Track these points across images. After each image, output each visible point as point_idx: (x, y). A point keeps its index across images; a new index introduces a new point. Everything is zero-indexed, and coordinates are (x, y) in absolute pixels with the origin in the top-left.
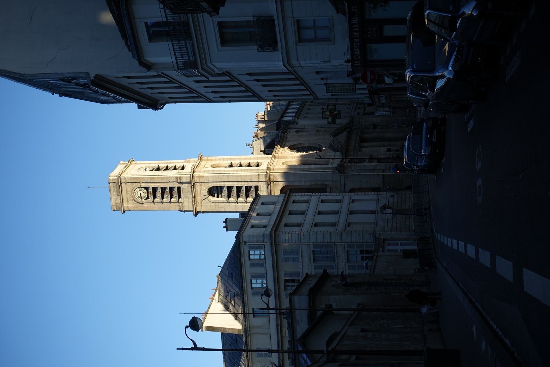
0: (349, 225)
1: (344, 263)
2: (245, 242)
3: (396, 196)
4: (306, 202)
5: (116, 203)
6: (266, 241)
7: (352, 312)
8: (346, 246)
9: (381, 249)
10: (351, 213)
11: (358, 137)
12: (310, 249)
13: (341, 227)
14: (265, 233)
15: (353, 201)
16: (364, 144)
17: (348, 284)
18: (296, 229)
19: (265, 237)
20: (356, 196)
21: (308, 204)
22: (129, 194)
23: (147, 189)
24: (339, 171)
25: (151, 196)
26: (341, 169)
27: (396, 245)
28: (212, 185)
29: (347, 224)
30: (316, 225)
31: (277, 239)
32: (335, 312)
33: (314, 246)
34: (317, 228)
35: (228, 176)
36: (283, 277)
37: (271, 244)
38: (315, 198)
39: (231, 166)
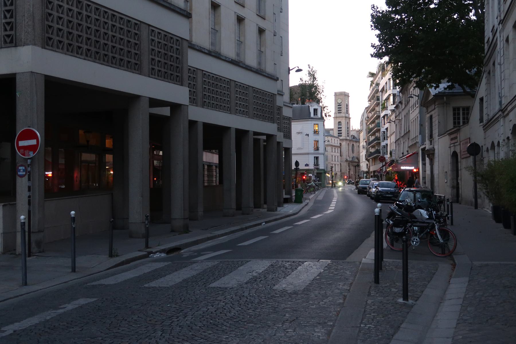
20: (339, 165)
38: (339, 154)
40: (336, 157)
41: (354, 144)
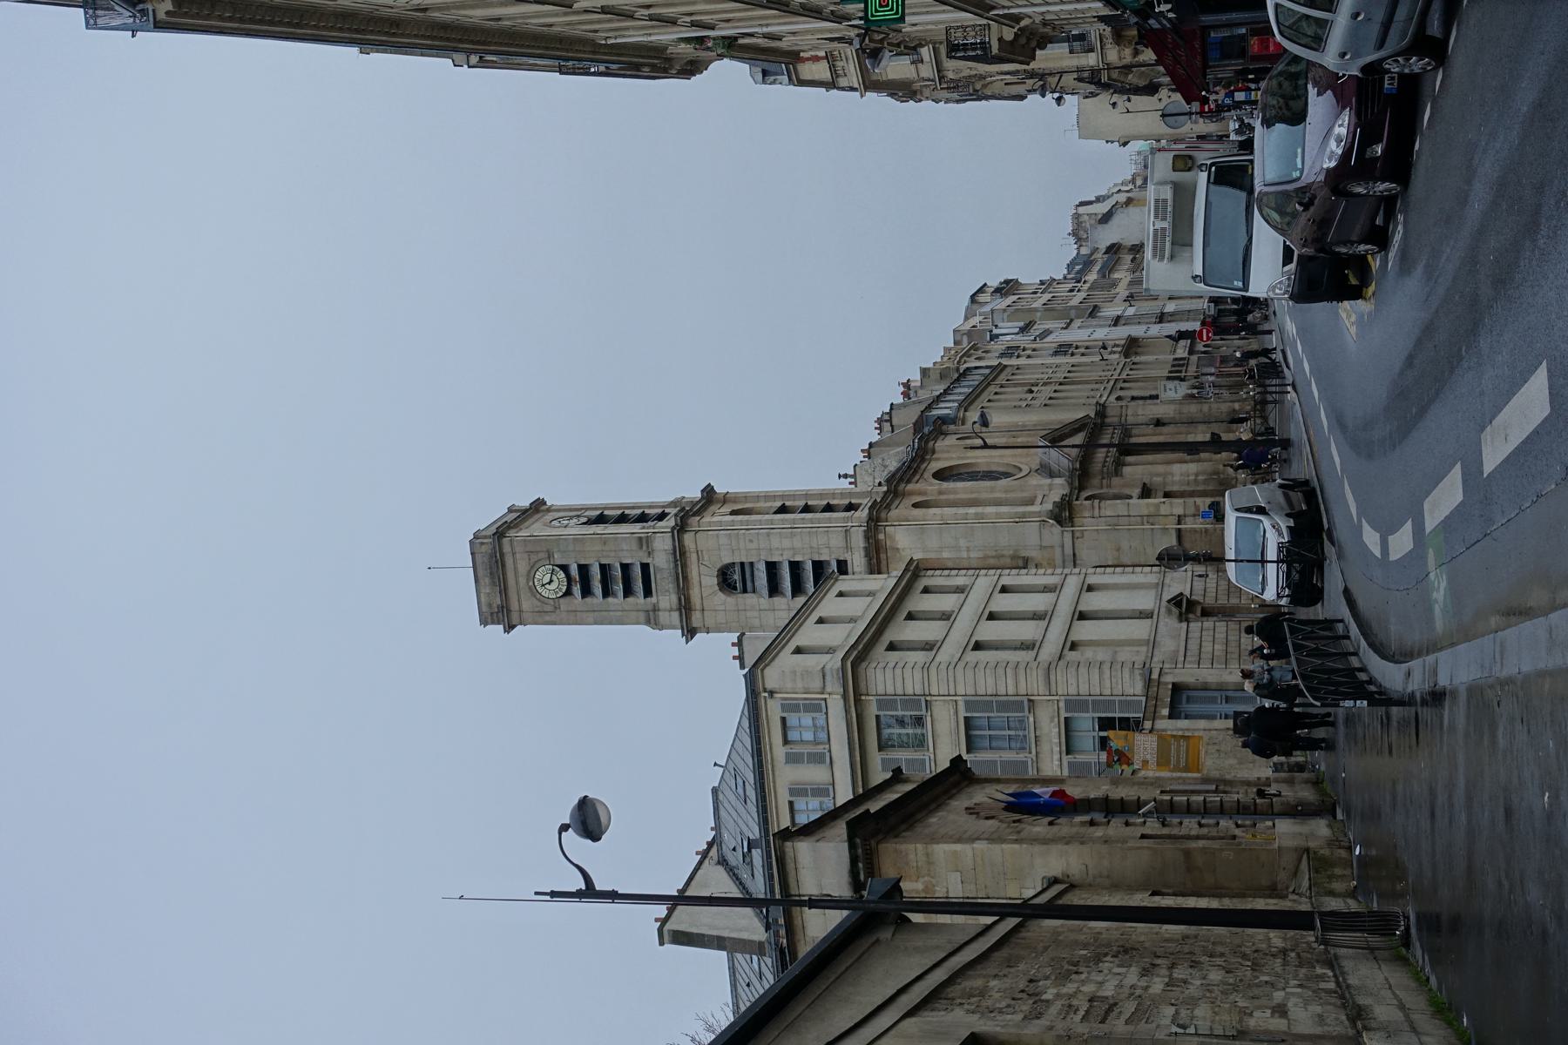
0: (1074, 646)
1: (1056, 756)
2: (771, 693)
4: (960, 590)
5: (490, 605)
6: (829, 689)
7: (989, 920)
8: (1062, 704)
9: (1165, 712)
10: (1083, 616)
12: (956, 712)
13: (1050, 649)
14: (828, 667)
15: (1090, 589)
16: (1129, 459)
17: (1032, 805)
18: (919, 657)
19: (828, 678)
21: (963, 596)
22: (522, 581)
23: (565, 568)
24: (1060, 521)
25: (577, 589)
26: (1063, 514)
27: (1213, 700)
29: (1068, 645)
30: (978, 646)
31: (862, 685)
32: (916, 918)
33: (969, 705)
34: (981, 655)
36: (872, 710)
37: (845, 697)
40: (1003, 603)
41: (936, 466)
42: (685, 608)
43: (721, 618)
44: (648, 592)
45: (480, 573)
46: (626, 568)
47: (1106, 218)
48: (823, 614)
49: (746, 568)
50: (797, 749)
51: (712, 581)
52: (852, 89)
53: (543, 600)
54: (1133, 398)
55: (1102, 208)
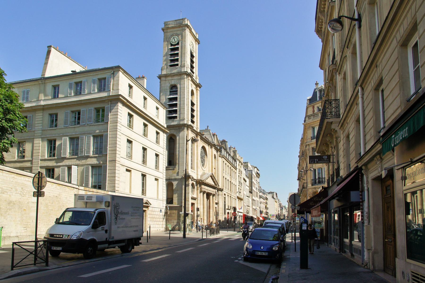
3: (161, 214)
11: (210, 192)
16: (205, 195)
22: (175, 32)
25: (173, 47)
28: (179, 86)
35: (184, 97)
39: (193, 104)
42: (166, 76)
43: (163, 85)
44: (171, 66)
45: (178, 21)
46: (177, 60)
47: (273, 197)
48: (134, 88)
49: (176, 92)
50: (265, 201)
51: (173, 83)
52: (305, 121)
53: (170, 38)
54: (225, 198)
55: (275, 197)
